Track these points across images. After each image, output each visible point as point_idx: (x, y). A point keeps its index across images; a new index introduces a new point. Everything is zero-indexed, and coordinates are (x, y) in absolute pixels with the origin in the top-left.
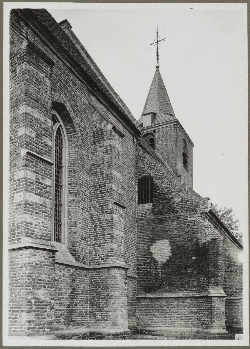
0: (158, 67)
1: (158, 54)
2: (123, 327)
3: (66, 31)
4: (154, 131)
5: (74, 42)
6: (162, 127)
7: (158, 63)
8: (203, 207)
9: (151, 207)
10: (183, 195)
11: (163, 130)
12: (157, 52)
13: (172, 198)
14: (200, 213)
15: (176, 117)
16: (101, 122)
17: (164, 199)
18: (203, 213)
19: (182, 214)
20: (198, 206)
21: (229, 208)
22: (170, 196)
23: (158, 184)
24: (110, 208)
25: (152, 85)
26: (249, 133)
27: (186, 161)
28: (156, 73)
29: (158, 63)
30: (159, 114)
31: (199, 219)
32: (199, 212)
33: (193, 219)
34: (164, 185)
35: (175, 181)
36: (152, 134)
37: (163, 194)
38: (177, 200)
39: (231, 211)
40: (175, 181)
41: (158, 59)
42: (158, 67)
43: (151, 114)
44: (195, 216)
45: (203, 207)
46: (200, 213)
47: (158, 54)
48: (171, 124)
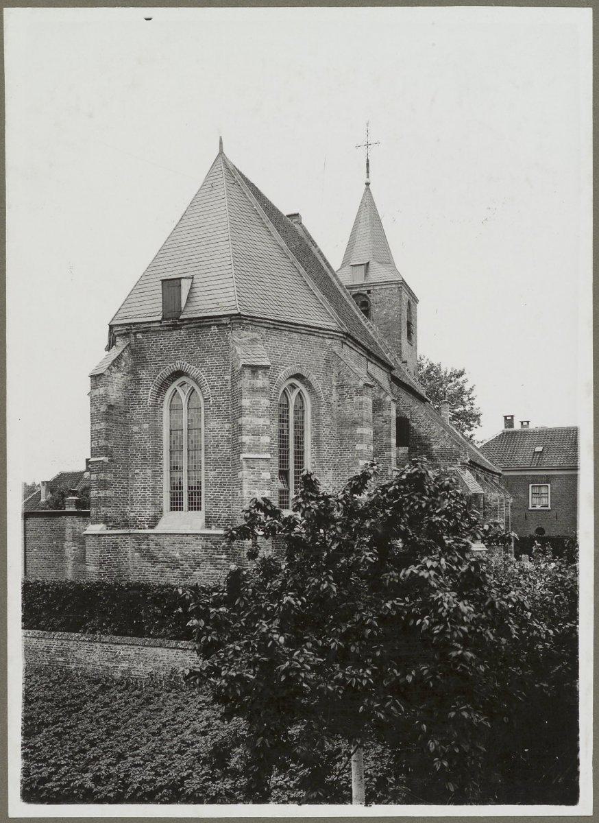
0: (368, 184)
1: (368, 164)
2: (183, 280)
3: (297, 226)
4: (369, 292)
5: (310, 244)
6: (380, 287)
7: (368, 177)
8: (464, 458)
9: (406, 451)
10: (443, 443)
11: (382, 292)
12: (368, 161)
13: (430, 444)
14: (461, 464)
15: (399, 266)
16: (380, 392)
17: (422, 444)
18: (464, 464)
19: (441, 462)
20: (458, 456)
21: (459, 369)
22: (428, 442)
23: (415, 428)
24: (389, 474)
25: (359, 212)
26: (595, 502)
27: (410, 333)
28: (365, 194)
29: (368, 177)
30: (373, 265)
31: (459, 470)
32: (459, 463)
33: (454, 469)
34: (421, 430)
35: (434, 427)
36: (365, 296)
37: (420, 438)
38: (435, 447)
39: (462, 374)
40: (434, 427)
41: (368, 172)
42: (368, 184)
43: (363, 266)
44: (456, 466)
45: (464, 458)
46: (461, 464)
47: (368, 164)
48: (394, 286)
